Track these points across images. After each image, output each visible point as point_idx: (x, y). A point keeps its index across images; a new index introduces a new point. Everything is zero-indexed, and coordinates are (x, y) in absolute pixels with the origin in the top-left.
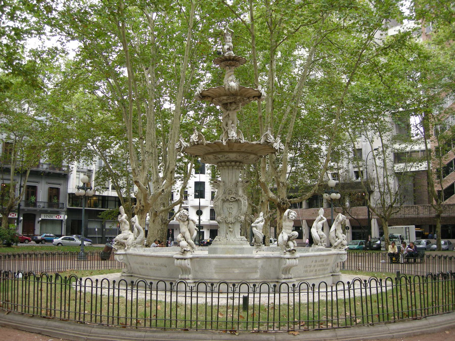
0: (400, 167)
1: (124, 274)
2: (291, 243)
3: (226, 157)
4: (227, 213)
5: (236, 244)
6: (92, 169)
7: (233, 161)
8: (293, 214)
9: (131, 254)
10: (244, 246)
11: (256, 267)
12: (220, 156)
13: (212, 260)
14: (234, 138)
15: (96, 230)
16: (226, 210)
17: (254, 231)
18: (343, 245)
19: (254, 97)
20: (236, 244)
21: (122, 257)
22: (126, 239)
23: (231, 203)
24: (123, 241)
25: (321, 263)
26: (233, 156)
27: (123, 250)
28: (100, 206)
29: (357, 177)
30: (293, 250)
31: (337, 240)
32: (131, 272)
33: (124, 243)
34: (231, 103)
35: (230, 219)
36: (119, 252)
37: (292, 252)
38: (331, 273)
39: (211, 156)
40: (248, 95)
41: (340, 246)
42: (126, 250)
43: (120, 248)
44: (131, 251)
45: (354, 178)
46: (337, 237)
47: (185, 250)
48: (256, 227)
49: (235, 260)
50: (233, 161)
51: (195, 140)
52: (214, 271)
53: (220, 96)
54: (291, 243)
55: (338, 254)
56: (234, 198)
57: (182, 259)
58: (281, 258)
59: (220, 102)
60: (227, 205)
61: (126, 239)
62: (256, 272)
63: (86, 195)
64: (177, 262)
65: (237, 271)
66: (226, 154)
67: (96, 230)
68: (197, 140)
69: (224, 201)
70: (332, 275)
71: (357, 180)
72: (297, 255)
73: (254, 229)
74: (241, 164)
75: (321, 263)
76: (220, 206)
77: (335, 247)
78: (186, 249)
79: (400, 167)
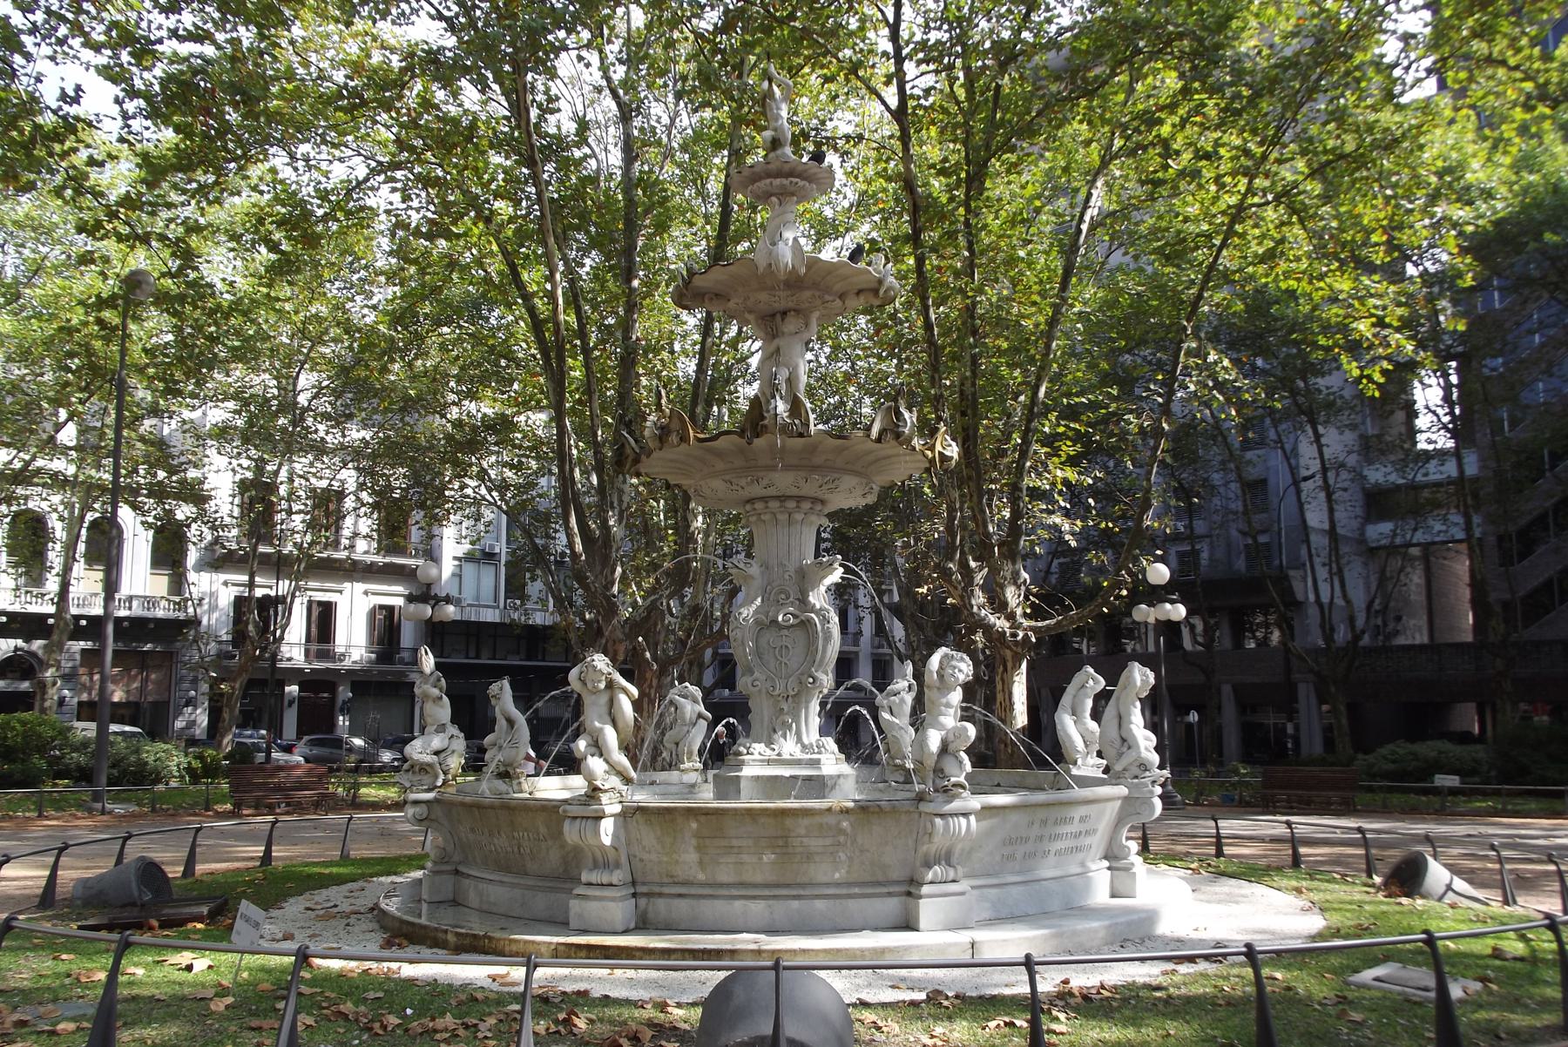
0: (1380, 531)
6: (497, 550)
12: (743, 482)
19: (859, 293)
23: (785, 632)
28: (121, 646)
40: (838, 287)
41: (1136, 771)
63: (435, 619)
66: (761, 474)
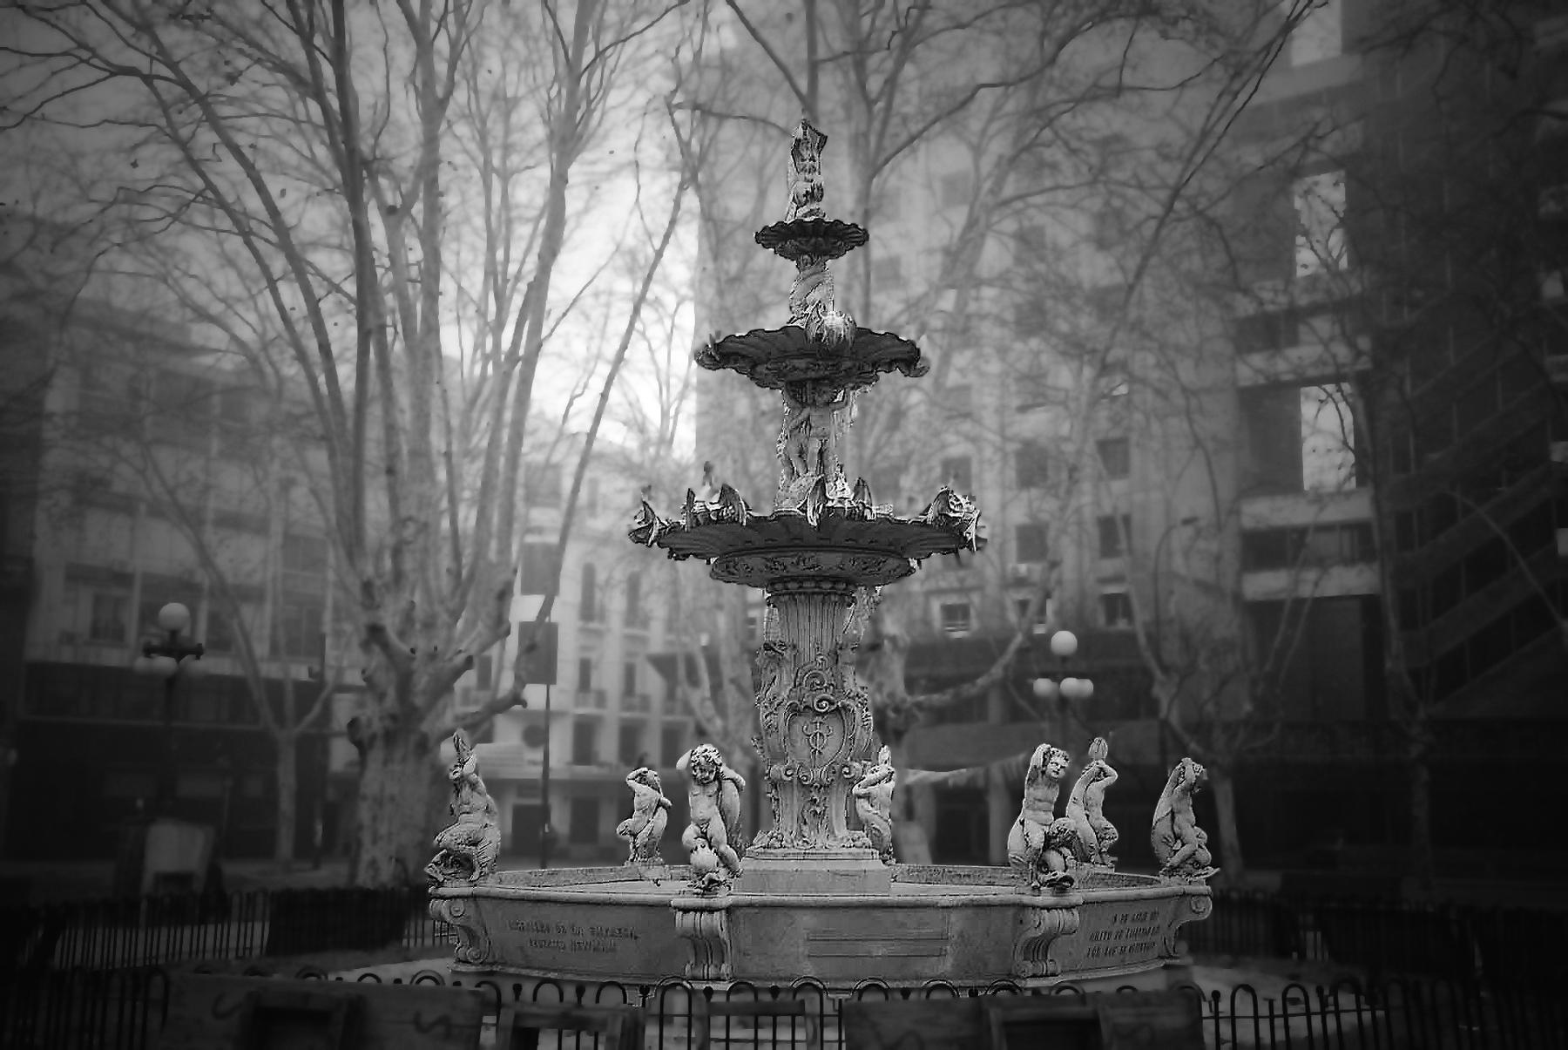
1: (462, 968)
2: (1054, 858)
3: (809, 564)
4: (806, 752)
5: (836, 858)
7: (826, 579)
8: (1061, 761)
9: (487, 897)
10: (864, 865)
11: (943, 938)
12: (788, 561)
13: (798, 914)
14: (847, 505)
15: (140, 803)
16: (801, 743)
17: (860, 812)
18: (1199, 865)
20: (836, 858)
21: (460, 906)
22: (475, 844)
24: (467, 849)
25: (1139, 925)
26: (830, 561)
27: (464, 883)
29: (1111, 618)
30: (1065, 879)
31: (1178, 845)
32: (490, 960)
33: (468, 859)
34: (816, 381)
35: (818, 774)
36: (449, 890)
37: (1061, 886)
38: (1161, 957)
39: (756, 562)
42: (473, 883)
43: (455, 876)
44: (491, 886)
45: (1101, 620)
46: (1177, 837)
47: (712, 881)
48: (867, 797)
49: (878, 913)
50: (826, 579)
51: (711, 508)
52: (803, 949)
53: (785, 355)
54: (1054, 858)
55: (1184, 895)
56: (831, 703)
57: (701, 910)
58: (1023, 907)
59: (780, 374)
60: (801, 723)
61: (475, 844)
62: (941, 954)
64: (684, 921)
65: (879, 950)
66: (807, 555)
67: (140, 803)
68: (717, 507)
69: (795, 711)
70: (1166, 967)
71: (1112, 629)
72: (1076, 896)
73: (863, 805)
74: (851, 588)
75: (1139, 925)
76: (783, 729)
77: (1173, 871)
78: (714, 876)
79: (1266, 584)
